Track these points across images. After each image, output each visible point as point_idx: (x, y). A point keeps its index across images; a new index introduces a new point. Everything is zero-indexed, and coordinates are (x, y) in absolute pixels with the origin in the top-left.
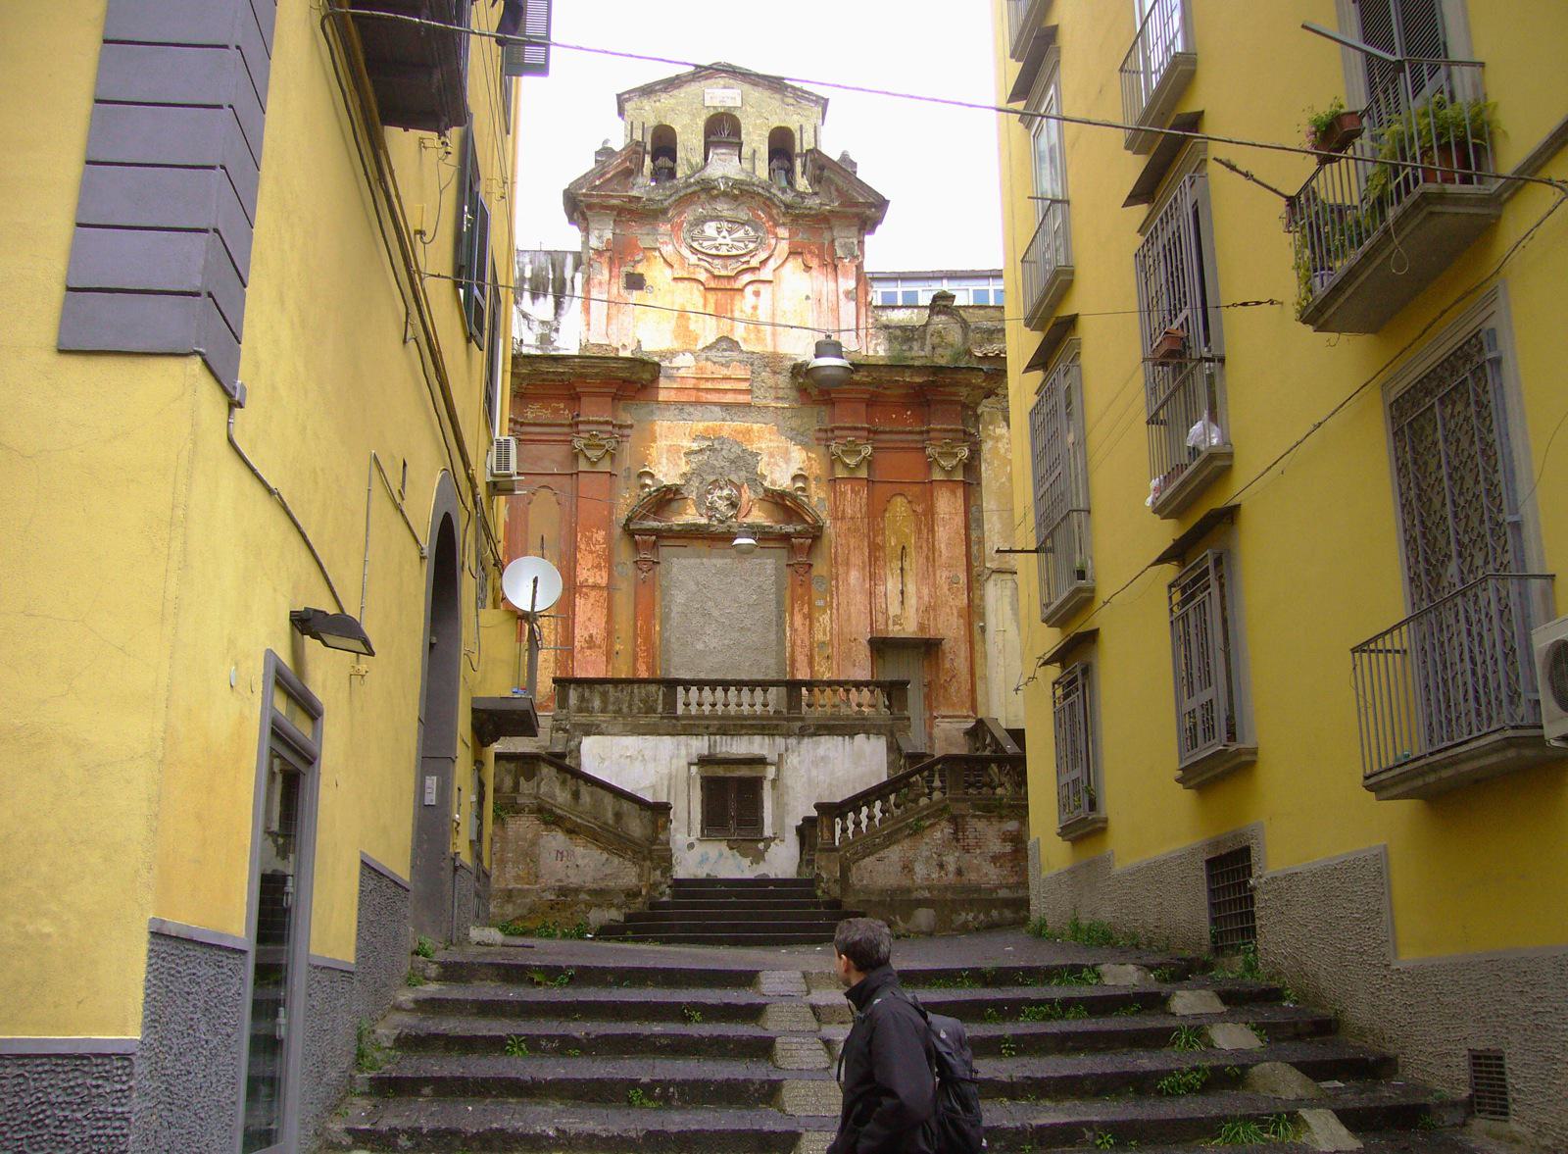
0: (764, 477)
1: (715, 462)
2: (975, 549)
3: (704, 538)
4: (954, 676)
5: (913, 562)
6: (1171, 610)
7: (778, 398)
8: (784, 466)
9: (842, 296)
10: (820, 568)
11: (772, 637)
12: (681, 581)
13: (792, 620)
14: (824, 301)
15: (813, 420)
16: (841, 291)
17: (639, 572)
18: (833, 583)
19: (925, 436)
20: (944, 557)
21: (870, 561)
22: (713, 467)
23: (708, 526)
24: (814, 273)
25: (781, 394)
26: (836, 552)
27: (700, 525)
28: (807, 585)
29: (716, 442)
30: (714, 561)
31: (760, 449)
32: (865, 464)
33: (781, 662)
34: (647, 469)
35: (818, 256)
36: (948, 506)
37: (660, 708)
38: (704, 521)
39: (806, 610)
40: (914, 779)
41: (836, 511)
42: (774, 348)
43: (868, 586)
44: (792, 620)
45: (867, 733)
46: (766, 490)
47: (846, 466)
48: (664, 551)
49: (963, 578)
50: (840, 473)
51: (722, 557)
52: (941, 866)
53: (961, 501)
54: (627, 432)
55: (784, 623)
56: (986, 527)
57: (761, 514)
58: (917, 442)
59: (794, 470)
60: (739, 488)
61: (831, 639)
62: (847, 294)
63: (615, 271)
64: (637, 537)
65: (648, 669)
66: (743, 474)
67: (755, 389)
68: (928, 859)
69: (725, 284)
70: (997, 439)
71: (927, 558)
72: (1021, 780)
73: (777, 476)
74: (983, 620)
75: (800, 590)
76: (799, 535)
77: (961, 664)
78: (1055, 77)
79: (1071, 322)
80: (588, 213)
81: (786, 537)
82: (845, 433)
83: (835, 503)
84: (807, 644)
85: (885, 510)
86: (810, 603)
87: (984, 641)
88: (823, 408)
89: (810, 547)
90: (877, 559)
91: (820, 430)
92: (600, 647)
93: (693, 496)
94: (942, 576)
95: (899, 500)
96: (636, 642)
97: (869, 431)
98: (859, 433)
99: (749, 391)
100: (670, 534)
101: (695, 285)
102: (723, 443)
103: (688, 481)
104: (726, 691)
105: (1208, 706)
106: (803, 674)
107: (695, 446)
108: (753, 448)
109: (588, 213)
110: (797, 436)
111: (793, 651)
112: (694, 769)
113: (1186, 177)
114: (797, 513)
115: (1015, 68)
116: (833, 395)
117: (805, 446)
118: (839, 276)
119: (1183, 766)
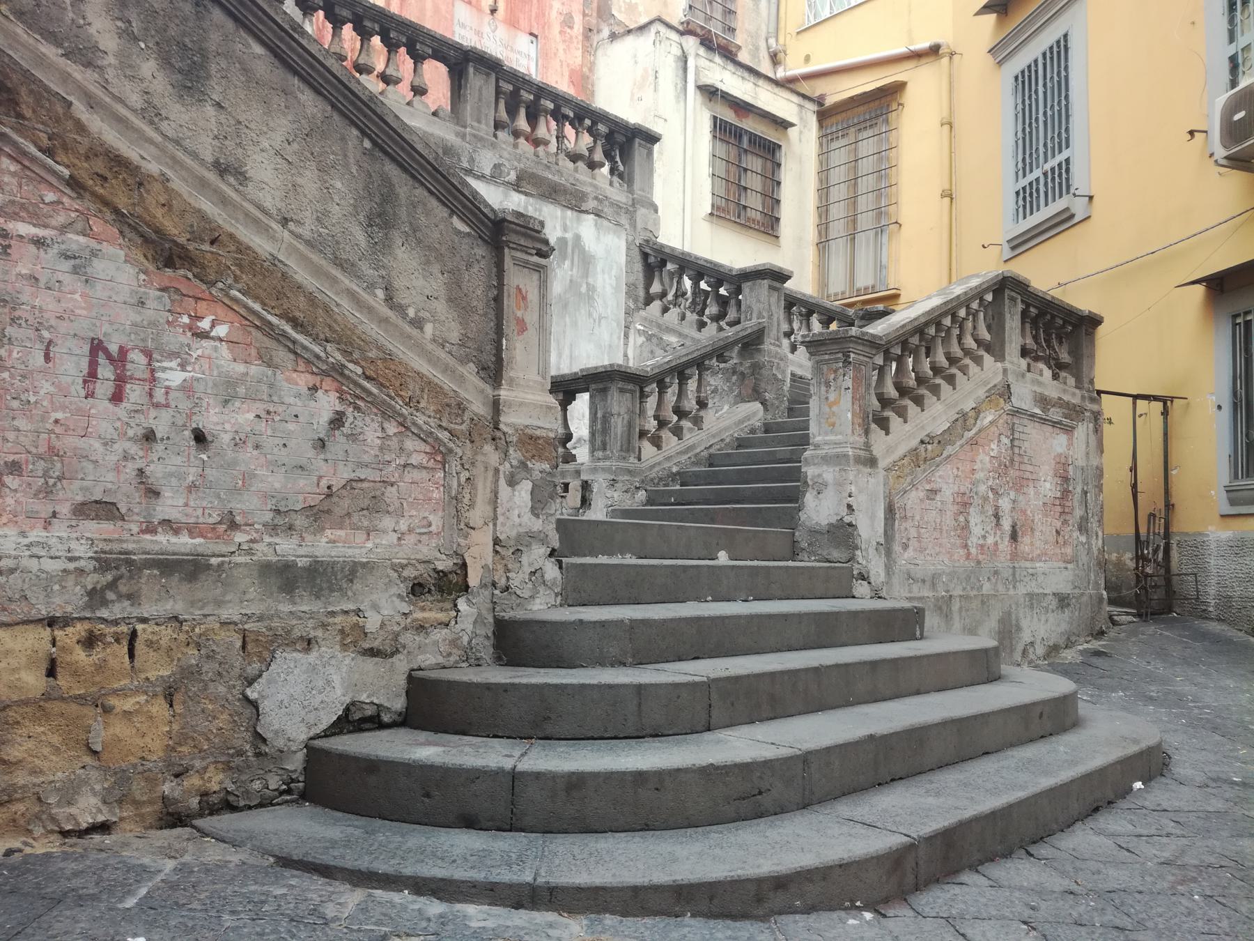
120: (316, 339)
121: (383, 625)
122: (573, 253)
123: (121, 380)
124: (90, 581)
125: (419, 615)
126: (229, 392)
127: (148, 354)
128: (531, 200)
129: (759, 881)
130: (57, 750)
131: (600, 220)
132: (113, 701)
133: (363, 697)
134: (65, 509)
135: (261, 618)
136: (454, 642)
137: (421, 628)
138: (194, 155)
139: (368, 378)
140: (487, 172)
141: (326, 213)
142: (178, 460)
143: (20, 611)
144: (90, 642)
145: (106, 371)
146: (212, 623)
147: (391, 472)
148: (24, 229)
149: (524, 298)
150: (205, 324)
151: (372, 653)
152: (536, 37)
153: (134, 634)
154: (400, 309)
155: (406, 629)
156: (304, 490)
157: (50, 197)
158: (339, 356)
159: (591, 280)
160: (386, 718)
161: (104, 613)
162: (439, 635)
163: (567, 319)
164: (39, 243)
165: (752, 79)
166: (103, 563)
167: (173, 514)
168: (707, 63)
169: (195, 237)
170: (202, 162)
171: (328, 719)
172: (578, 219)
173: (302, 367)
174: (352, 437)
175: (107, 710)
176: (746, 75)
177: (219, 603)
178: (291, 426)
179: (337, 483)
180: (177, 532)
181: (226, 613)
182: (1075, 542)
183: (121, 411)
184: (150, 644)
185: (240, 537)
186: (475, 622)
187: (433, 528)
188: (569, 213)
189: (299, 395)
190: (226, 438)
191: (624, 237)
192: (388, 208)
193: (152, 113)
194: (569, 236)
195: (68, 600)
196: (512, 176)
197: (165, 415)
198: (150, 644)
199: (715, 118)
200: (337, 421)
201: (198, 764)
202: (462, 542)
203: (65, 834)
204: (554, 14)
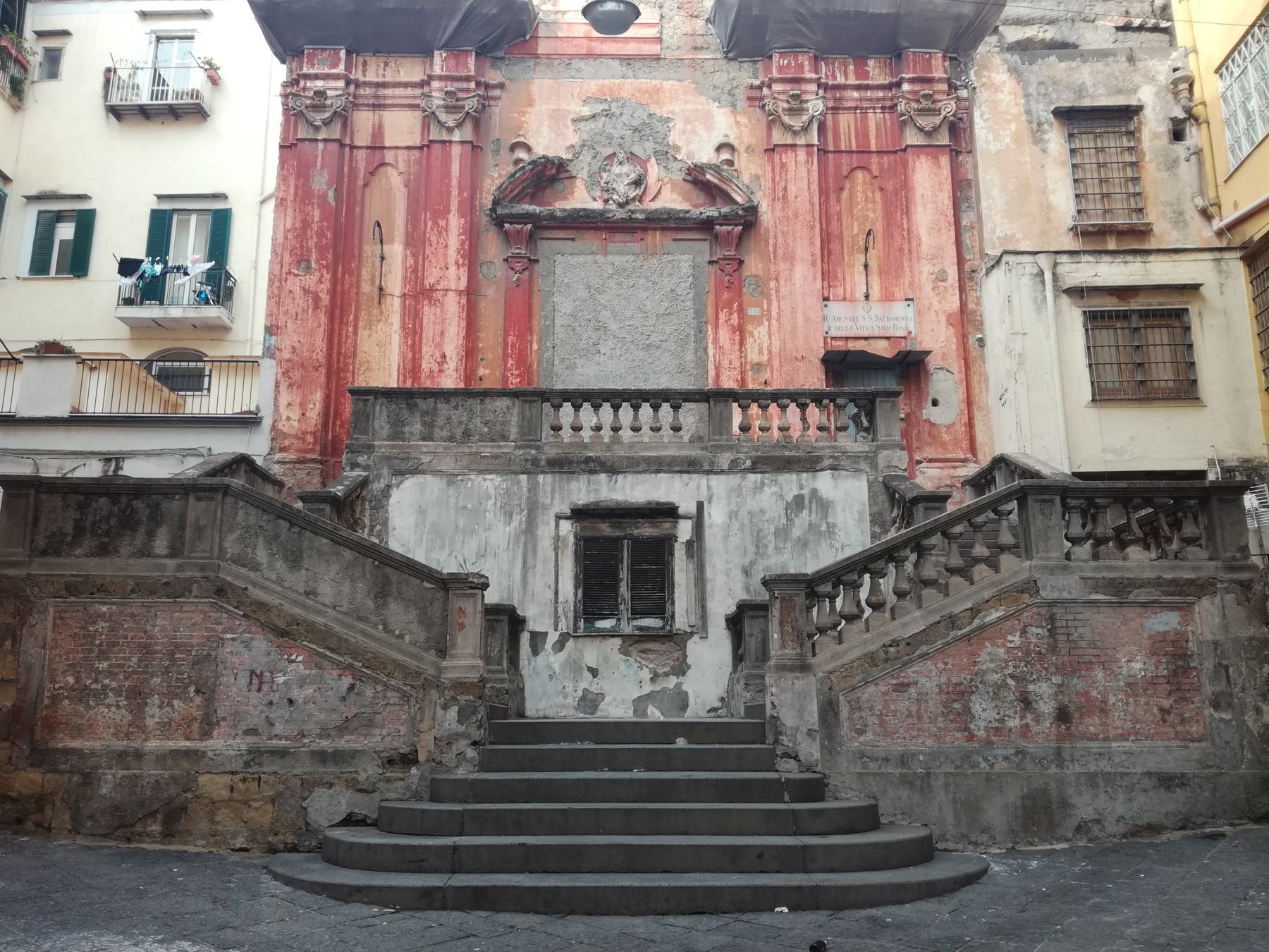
0: (677, 149)
1: (612, 131)
2: (966, 238)
3: (597, 229)
7: (695, 48)
10: (753, 265)
11: (690, 356)
12: (567, 285)
17: (512, 272)
21: (822, 255)
22: (610, 137)
26: (775, 244)
27: (593, 211)
28: (735, 287)
29: (614, 105)
30: (610, 258)
31: (673, 112)
34: (522, 139)
37: (514, 432)
38: (598, 205)
39: (735, 319)
47: (788, 128)
48: (544, 246)
52: (1026, 702)
54: (497, 93)
55: (705, 337)
56: (984, 204)
59: (718, 139)
60: (643, 163)
61: (770, 360)
64: (507, 225)
66: (650, 146)
67: (664, 37)
73: (694, 147)
74: (981, 330)
75: (726, 295)
76: (725, 220)
81: (706, 226)
83: (773, 180)
86: (741, 311)
89: (741, 237)
93: (584, 174)
96: (506, 363)
99: (659, 40)
100: (552, 224)
102: (622, 106)
103: (576, 155)
107: (586, 111)
112: (566, 527)
120: (340, 655)
121: (367, 778)
122: (810, 503)
123: (261, 683)
124: (245, 758)
125: (388, 774)
126: (302, 682)
127: (271, 672)
128: (767, 475)
129: (350, 887)
130: (232, 820)
131: (836, 473)
132: (251, 803)
133: (357, 811)
134: (240, 732)
135: (310, 774)
136: (408, 788)
137: (388, 780)
138: (296, 591)
139: (366, 667)
140: (725, 467)
141: (354, 599)
142: (282, 711)
143: (221, 769)
144: (244, 780)
145: (255, 681)
146: (289, 775)
147: (379, 708)
148: (229, 636)
149: (464, 612)
150: (293, 657)
151: (361, 791)
152: (912, 300)
153: (260, 778)
154: (391, 632)
155: (380, 780)
156: (336, 719)
157: (238, 623)
158: (351, 661)
159: (830, 520)
160: (369, 821)
161: (250, 770)
162: (399, 784)
163: (808, 554)
164: (233, 639)
165: (1139, 259)
166: (250, 752)
167: (279, 732)
168: (1075, 266)
169: (289, 625)
170: (299, 594)
171: (338, 819)
172: (814, 477)
173: (335, 667)
174: (359, 694)
175: (250, 806)
176: (1129, 258)
177: (293, 767)
178: (330, 693)
179: (350, 716)
180: (280, 739)
181: (295, 772)
182: (1208, 720)
183: (260, 695)
184: (265, 782)
185: (306, 741)
186: (420, 779)
187: (402, 733)
188: (804, 475)
189: (333, 679)
190: (301, 701)
191: (864, 478)
192: (387, 588)
193: (280, 581)
194: (806, 492)
195: (238, 765)
196: (748, 463)
197: (277, 694)
198: (265, 782)
199: (1085, 312)
200: (352, 688)
201: (282, 831)
202: (415, 739)
203: (233, 850)
204: (924, 277)
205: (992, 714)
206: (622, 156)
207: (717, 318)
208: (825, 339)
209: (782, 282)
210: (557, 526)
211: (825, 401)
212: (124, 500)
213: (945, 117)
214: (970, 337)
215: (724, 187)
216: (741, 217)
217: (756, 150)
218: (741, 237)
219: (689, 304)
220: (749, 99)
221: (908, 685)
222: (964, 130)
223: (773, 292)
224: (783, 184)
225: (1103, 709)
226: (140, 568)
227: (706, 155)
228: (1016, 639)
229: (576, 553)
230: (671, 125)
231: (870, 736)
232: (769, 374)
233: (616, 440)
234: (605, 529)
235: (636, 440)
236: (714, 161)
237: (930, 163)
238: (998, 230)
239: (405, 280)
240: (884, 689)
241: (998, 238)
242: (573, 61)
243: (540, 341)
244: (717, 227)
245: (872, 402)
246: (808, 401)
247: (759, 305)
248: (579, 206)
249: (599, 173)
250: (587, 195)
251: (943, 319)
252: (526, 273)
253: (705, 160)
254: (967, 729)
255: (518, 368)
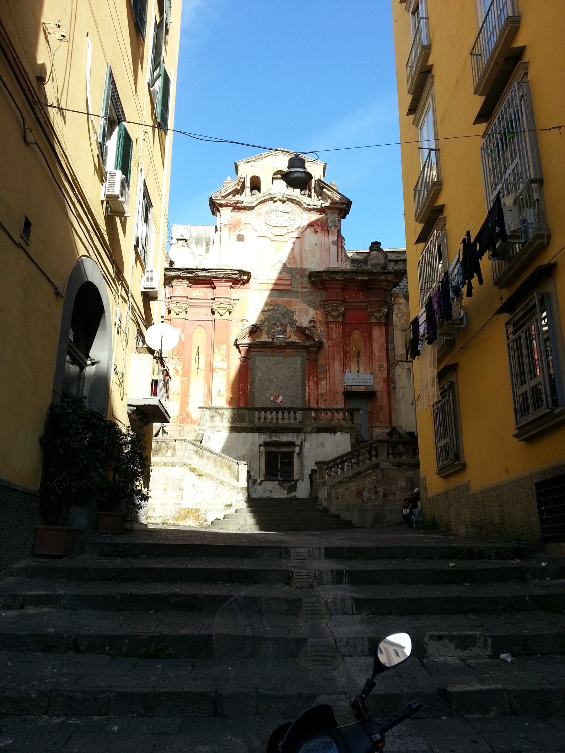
0: (297, 321)
1: (275, 315)
2: (390, 354)
4: (382, 409)
5: (363, 358)
6: (508, 338)
8: (305, 316)
9: (331, 244)
10: (321, 361)
13: (309, 383)
14: (323, 245)
15: (318, 297)
16: (330, 242)
18: (327, 367)
19: (368, 303)
20: (376, 356)
21: (344, 358)
22: (274, 317)
23: (272, 343)
24: (319, 234)
25: (304, 285)
26: (328, 354)
29: (276, 306)
30: (274, 358)
31: (295, 309)
32: (341, 316)
33: (304, 403)
35: (320, 226)
36: (378, 334)
38: (270, 340)
39: (315, 379)
40: (362, 451)
41: (329, 336)
42: (301, 265)
43: (342, 368)
44: (309, 383)
45: (341, 432)
46: (297, 327)
47: (333, 316)
49: (385, 365)
50: (330, 319)
51: (278, 356)
52: (376, 493)
53: (384, 331)
54: (236, 302)
57: (295, 337)
58: (364, 306)
59: (310, 318)
61: (326, 393)
62: (333, 242)
63: (232, 233)
65: (244, 403)
66: (287, 320)
67: (293, 284)
68: (370, 489)
69: (279, 238)
70: (400, 304)
71: (369, 357)
72: (415, 453)
73: (302, 321)
75: (312, 371)
76: (312, 346)
77: (385, 403)
78: (432, 92)
79: (441, 209)
80: (220, 209)
81: (306, 347)
82: (332, 302)
83: (328, 332)
84: (316, 394)
85: (350, 336)
86: (317, 376)
87: (395, 393)
88: (323, 292)
89: (317, 351)
90: (347, 357)
91: (321, 301)
92: (223, 395)
93: (266, 330)
94: (376, 364)
95: (357, 331)
97: (343, 301)
98: (338, 302)
99: (290, 285)
101: (269, 239)
103: (263, 323)
104: (277, 413)
105: (535, 390)
106: (314, 405)
108: (292, 309)
109: (220, 209)
110: (311, 304)
111: (309, 397)
112: (262, 448)
113: (515, 84)
114: (311, 336)
115: (410, 97)
116: (327, 286)
117: (315, 308)
118: (330, 235)
119: (518, 426)
174: (218, 490)
205: (368, 495)
206: (278, 324)
207: (309, 379)
208: (344, 386)
209: (330, 367)
210: (260, 448)
211: (339, 411)
212: (160, 443)
213: (384, 313)
214: (391, 386)
215: (312, 335)
216: (317, 345)
217: (323, 322)
218: (317, 351)
219: (300, 373)
220: (320, 305)
221: (349, 488)
222: (391, 316)
223: (327, 370)
224: (331, 334)
225: (395, 494)
226: (164, 459)
227: (306, 324)
228: (374, 477)
229: (265, 456)
230: (294, 313)
231: (339, 500)
232: (326, 397)
233: (277, 422)
234: (274, 449)
235: (283, 423)
236: (308, 326)
237: (378, 328)
238: (399, 351)
239: (206, 365)
240: (343, 489)
241: (400, 354)
242: (262, 291)
243: (250, 386)
244: (309, 348)
245: (353, 411)
246: (334, 411)
247: (323, 374)
248: (264, 340)
249: (271, 329)
250: (266, 336)
251: (382, 380)
252: (246, 362)
253: (305, 326)
254: (362, 499)
255: (243, 395)
